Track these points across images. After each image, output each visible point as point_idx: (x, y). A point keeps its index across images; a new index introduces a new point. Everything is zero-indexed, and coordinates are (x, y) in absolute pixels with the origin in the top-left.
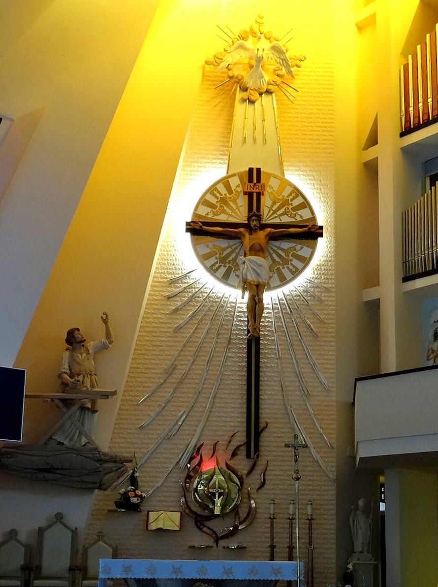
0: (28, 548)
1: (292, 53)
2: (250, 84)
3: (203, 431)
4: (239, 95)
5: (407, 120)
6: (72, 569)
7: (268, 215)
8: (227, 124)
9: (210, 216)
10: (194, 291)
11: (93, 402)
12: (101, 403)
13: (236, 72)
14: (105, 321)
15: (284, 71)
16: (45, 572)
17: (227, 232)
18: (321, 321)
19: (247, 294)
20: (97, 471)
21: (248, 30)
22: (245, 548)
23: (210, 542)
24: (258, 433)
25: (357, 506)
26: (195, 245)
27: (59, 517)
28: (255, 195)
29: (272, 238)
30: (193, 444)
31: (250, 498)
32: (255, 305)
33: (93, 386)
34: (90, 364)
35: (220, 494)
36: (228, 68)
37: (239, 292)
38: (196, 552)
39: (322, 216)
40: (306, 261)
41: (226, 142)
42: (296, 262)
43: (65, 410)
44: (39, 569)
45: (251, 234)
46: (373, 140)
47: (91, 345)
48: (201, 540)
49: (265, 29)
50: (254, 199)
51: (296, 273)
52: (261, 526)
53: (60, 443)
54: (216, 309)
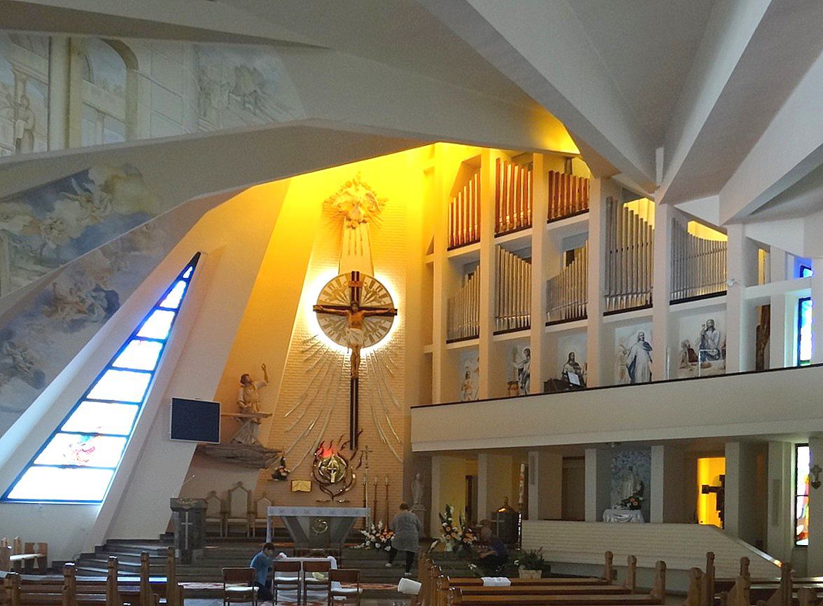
0: (222, 502)
1: (379, 196)
2: (352, 216)
3: (324, 433)
4: (346, 223)
5: (452, 241)
6: (249, 513)
7: (364, 302)
8: (327, 351)
9: (328, 301)
10: (318, 348)
11: (258, 420)
12: (263, 420)
13: (344, 208)
14: (264, 369)
15: (374, 209)
16: (233, 515)
17: (339, 310)
18: (397, 368)
19: (351, 350)
20: (261, 458)
21: (351, 181)
22: (349, 501)
23: (329, 498)
24: (357, 436)
25: (415, 477)
26: (319, 318)
27: (240, 484)
28: (356, 289)
29: (366, 315)
30: (318, 441)
31: (352, 473)
32: (355, 358)
33: (258, 410)
34: (255, 396)
35: (335, 471)
36: (339, 206)
37: (346, 348)
38: (320, 503)
39: (398, 301)
40: (387, 330)
41: (338, 252)
42: (381, 331)
43: (242, 423)
44: (229, 512)
45: (352, 314)
46: (431, 251)
47: (256, 383)
48: (323, 497)
49: (363, 181)
50: (355, 292)
51: (381, 337)
52: (359, 490)
53: (239, 442)
54: (332, 359)
